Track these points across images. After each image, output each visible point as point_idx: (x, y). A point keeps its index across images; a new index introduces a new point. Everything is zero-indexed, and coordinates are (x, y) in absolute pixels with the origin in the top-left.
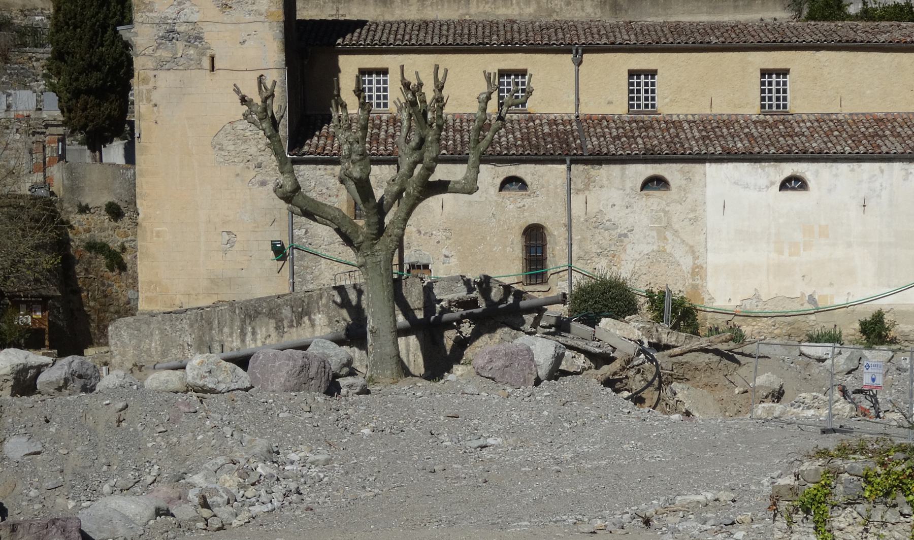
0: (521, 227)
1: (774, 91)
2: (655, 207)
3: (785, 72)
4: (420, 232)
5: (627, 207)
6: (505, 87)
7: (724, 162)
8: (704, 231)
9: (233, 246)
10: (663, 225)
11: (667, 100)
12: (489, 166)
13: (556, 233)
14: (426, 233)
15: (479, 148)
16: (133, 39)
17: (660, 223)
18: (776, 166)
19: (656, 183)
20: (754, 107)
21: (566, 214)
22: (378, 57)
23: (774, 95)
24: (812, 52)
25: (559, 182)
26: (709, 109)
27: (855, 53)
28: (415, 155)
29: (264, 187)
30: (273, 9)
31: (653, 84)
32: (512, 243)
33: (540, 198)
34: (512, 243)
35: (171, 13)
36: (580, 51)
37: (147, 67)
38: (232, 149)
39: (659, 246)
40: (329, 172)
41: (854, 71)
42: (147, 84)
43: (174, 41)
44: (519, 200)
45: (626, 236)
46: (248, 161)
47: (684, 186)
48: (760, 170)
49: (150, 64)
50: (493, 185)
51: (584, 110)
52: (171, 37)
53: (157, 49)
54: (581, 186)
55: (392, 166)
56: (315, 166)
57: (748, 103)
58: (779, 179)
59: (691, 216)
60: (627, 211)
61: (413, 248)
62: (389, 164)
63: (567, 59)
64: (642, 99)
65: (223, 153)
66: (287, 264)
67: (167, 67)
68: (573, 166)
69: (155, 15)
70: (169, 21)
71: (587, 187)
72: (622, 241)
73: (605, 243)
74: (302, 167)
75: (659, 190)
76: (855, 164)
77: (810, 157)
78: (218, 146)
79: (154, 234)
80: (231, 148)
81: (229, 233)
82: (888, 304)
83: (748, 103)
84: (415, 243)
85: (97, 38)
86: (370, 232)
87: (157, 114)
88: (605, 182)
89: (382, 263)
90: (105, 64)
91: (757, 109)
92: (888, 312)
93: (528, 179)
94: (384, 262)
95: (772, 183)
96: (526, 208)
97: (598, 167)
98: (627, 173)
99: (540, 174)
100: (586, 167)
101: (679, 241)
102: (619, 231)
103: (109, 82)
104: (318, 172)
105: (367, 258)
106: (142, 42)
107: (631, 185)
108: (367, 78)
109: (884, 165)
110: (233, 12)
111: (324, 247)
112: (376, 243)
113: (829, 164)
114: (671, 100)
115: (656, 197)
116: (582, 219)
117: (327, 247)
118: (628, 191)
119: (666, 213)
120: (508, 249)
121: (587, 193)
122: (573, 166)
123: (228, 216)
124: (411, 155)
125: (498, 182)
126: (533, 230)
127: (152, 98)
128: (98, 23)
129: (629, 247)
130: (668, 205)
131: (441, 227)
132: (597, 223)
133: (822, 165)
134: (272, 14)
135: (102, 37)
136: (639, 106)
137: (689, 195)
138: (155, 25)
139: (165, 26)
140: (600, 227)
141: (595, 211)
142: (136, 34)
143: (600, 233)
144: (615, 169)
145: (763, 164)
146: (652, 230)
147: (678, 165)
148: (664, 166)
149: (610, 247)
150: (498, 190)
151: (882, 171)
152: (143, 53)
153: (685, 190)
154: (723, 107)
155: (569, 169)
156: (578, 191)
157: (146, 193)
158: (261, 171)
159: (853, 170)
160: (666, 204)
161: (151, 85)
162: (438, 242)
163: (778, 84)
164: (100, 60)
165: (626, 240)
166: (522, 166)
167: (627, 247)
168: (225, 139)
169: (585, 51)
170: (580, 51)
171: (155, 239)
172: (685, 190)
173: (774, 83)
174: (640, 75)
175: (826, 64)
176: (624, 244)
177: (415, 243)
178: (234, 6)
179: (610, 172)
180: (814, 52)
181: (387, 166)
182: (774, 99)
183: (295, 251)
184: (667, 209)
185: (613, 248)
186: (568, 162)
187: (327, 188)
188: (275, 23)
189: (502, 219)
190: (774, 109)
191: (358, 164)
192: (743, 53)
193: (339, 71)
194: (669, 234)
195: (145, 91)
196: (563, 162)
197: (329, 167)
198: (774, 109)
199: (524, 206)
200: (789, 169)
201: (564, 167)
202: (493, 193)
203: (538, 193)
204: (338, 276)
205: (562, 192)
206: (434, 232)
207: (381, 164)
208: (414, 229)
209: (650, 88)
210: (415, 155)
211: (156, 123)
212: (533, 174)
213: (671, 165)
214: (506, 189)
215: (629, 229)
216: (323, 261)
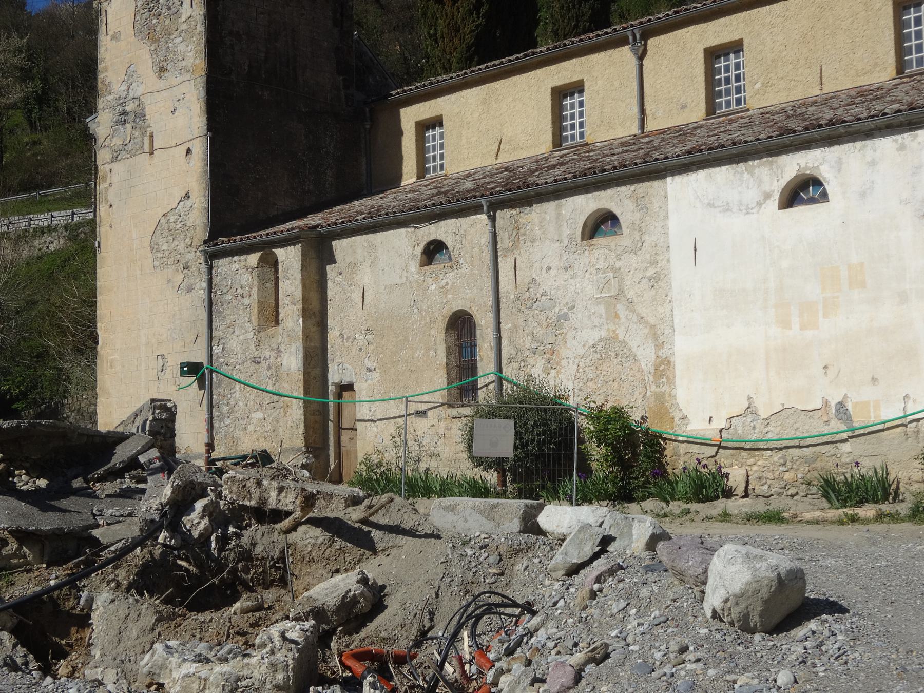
2: (601, 265)
5: (566, 269)
7: (692, 171)
10: (613, 294)
11: (758, 86)
12: (409, 229)
14: (349, 338)
20: (886, 69)
30: (198, 61)
33: (463, 270)
34: (435, 344)
40: (243, 264)
47: (638, 222)
48: (746, 175)
59: (650, 273)
71: (515, 246)
83: (876, 64)
95: (767, 196)
96: (448, 287)
97: (528, 209)
100: (514, 212)
101: (635, 319)
114: (763, 84)
116: (512, 297)
119: (616, 270)
137: (646, 237)
141: (527, 281)
145: (751, 163)
147: (628, 187)
150: (418, 265)
155: (493, 219)
159: (902, 148)
172: (640, 229)
174: (729, 54)
176: (565, 331)
181: (292, 247)
183: (214, 375)
199: (447, 284)
201: (483, 217)
205: (487, 256)
208: (338, 334)
216: (238, 385)
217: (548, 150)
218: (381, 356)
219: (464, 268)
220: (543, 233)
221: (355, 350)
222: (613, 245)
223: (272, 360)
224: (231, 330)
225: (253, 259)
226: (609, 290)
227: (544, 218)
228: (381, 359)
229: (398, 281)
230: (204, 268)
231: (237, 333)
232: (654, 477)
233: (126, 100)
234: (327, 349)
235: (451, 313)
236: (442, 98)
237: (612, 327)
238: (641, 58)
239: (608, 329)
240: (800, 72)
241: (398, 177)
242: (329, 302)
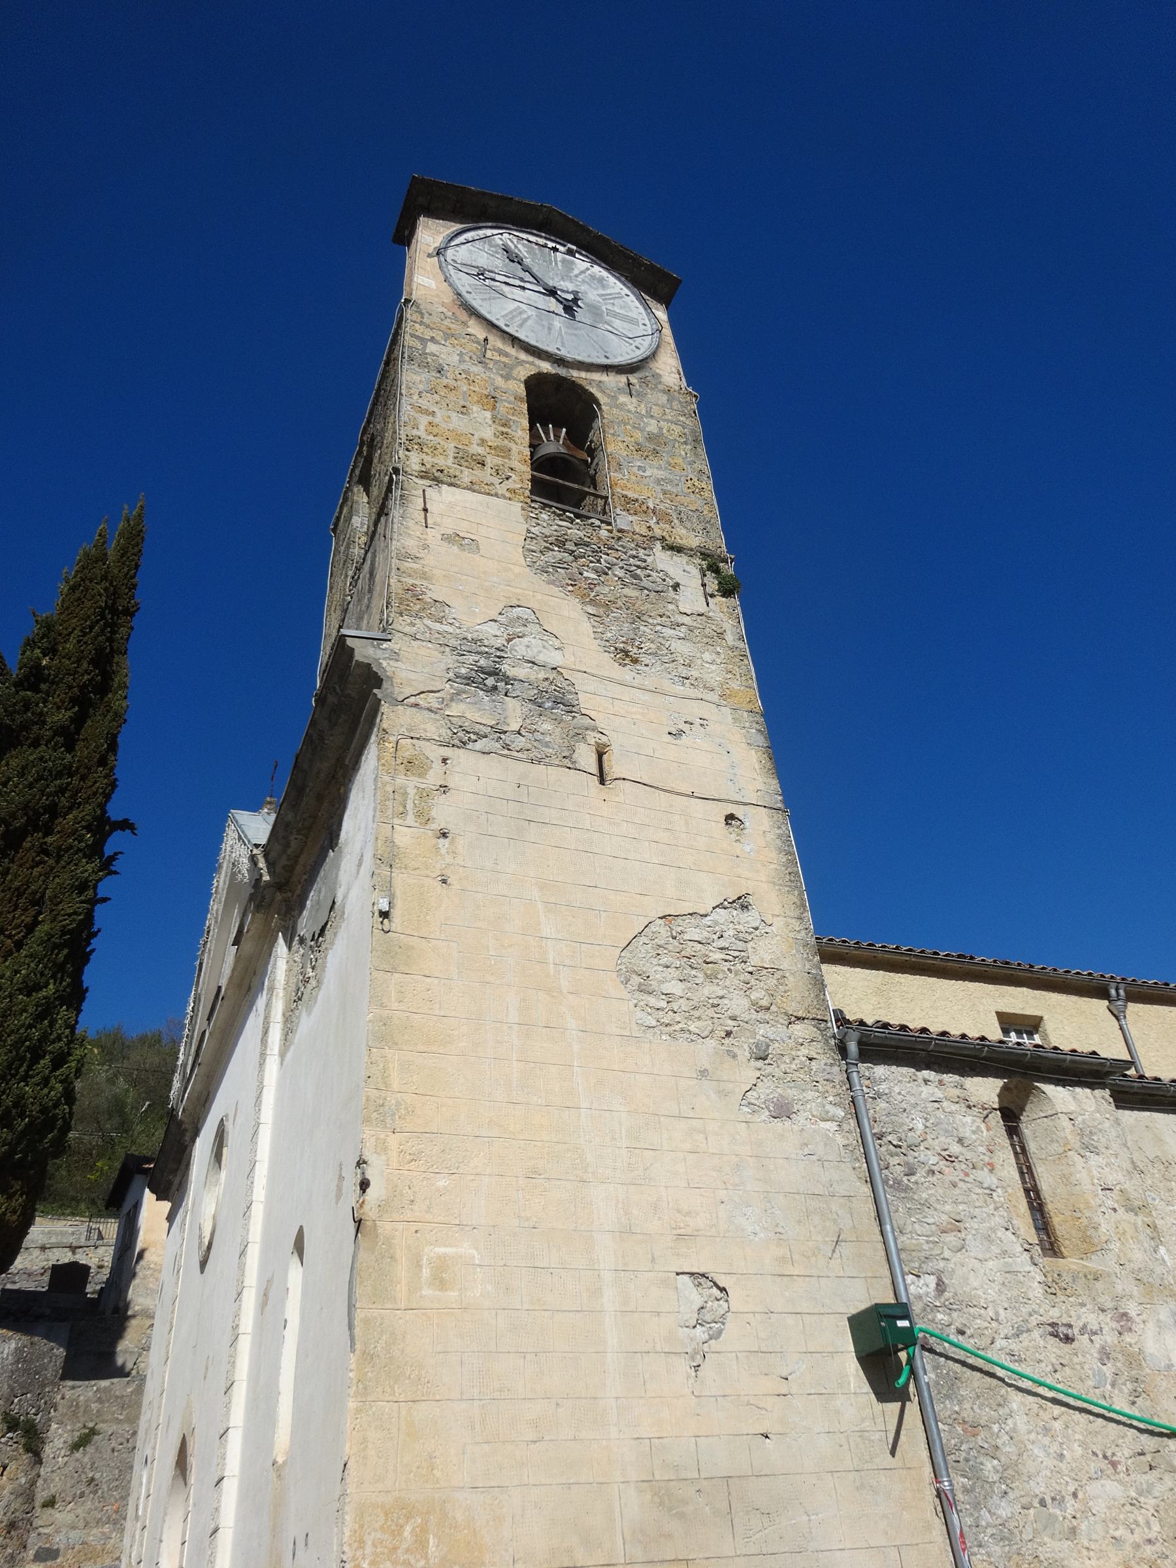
9: (720, 1332)
16: (384, 664)
35: (493, 634)
38: (679, 992)
46: (728, 1034)
49: (433, 728)
53: (452, 700)
55: (1098, 1092)
56: (913, 1070)
58: (1105, 1367)
65: (652, 1001)
66: (912, 1408)
67: (479, 745)
74: (880, 1070)
78: (636, 980)
79: (426, 1272)
80: (676, 988)
85: (21, 1066)
87: (449, 859)
90: (22, 1115)
103: (21, 1152)
106: (412, 676)
111: (1004, 1343)
123: (688, 1214)
127: (433, 813)
128: (27, 1043)
135: (30, 1068)
138: (447, 649)
142: (395, 656)
152: (412, 700)
157: (398, 1104)
158: (769, 1069)
161: (434, 777)
164: (16, 1105)
168: (655, 961)
171: (426, 1292)
181: (1088, 1091)
188: (745, 714)
195: (412, 792)
211: (444, 882)
216: (1016, 1399)
225: (987, 1089)
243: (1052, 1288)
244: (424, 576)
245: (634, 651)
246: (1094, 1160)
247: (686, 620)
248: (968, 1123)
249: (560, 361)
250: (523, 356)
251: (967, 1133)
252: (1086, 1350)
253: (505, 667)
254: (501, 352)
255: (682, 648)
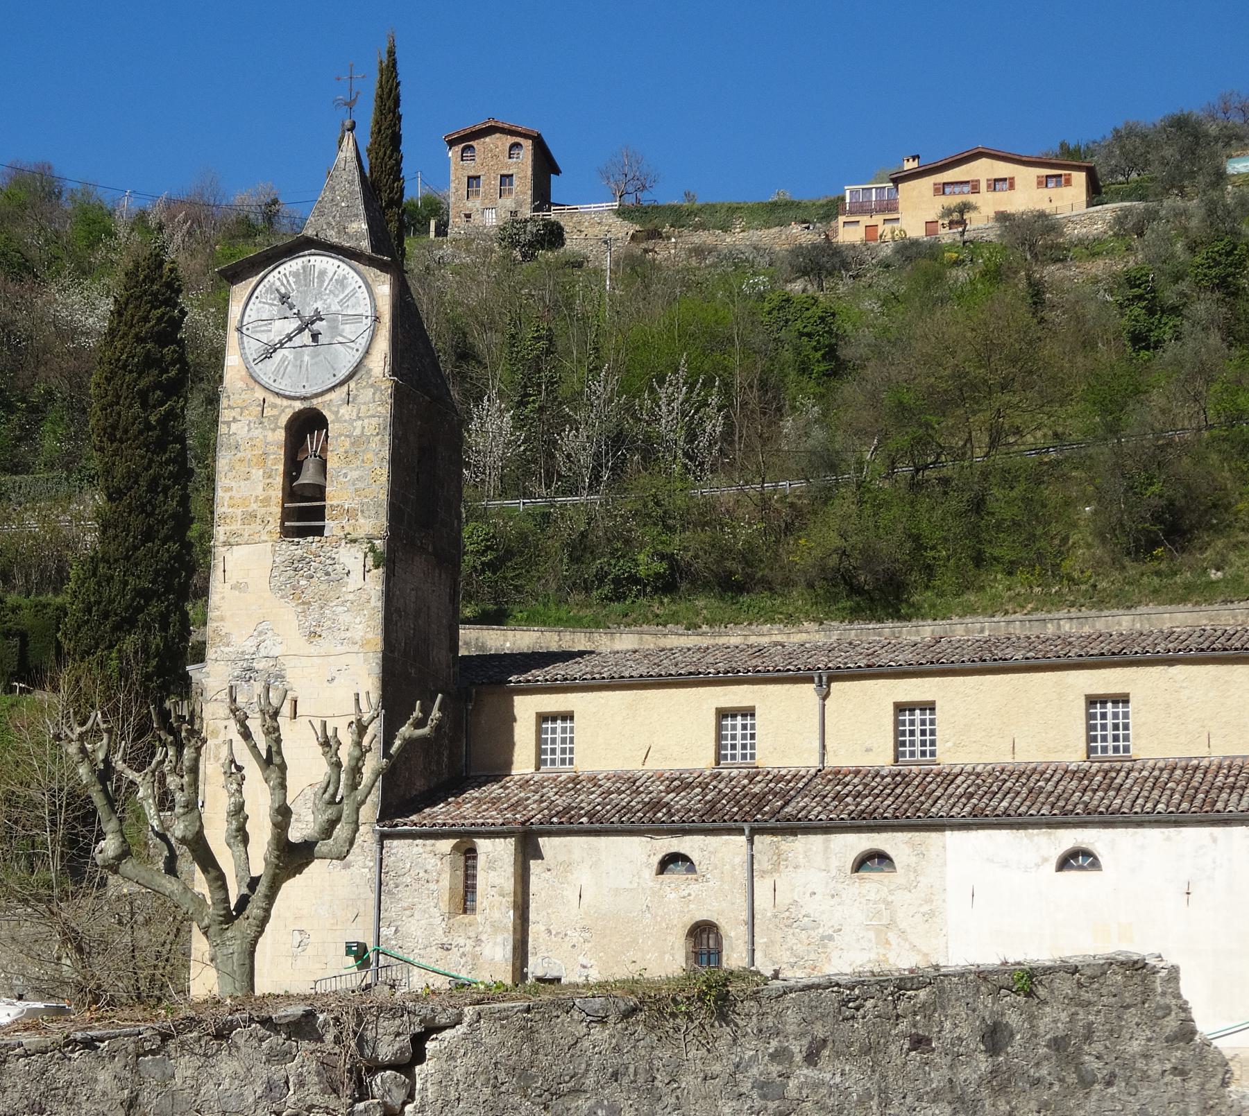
0: (684, 926)
1: (1110, 727)
2: (872, 896)
3: (1123, 699)
4: (550, 932)
5: (833, 896)
6: (729, 733)
7: (972, 829)
8: (944, 932)
10: (884, 922)
11: (949, 744)
12: (644, 839)
13: (732, 934)
14: (558, 933)
15: (356, 797)
17: (880, 919)
18: (1050, 833)
19: (873, 860)
20: (1076, 751)
21: (745, 905)
22: (554, 697)
23: (1110, 733)
24: (1162, 667)
25: (737, 860)
26: (1011, 756)
27: (1230, 666)
28: (330, 811)
29: (348, 870)
30: (370, 636)
31: (932, 722)
32: (673, 948)
33: (711, 884)
34: (673, 948)
35: (249, 646)
36: (824, 679)
37: (217, 716)
39: (878, 953)
40: (429, 848)
41: (1229, 693)
42: (217, 738)
43: (252, 681)
44: (683, 887)
45: (830, 938)
47: (913, 865)
48: (1025, 839)
50: (648, 865)
51: (832, 762)
52: (247, 676)
54: (767, 866)
57: (1067, 746)
59: (925, 908)
60: (833, 902)
61: (540, 955)
62: (505, 838)
63: (808, 691)
64: (918, 743)
68: (756, 838)
69: (231, 649)
70: (246, 657)
71: (776, 867)
72: (825, 946)
73: (800, 949)
74: (396, 843)
75: (882, 871)
76: (1172, 830)
77: (1097, 819)
81: (301, 931)
82: (1231, 1048)
83: (1067, 746)
84: (543, 948)
86: (216, 912)
88: (801, 860)
89: (236, 954)
91: (1081, 754)
92: (1231, 1060)
93: (694, 857)
94: (239, 954)
95: (1045, 860)
96: (691, 898)
97: (792, 838)
98: (832, 846)
99: (711, 849)
100: (775, 839)
101: (907, 946)
102: (821, 930)
104: (415, 850)
105: (217, 948)
107: (837, 864)
108: (549, 725)
109: (1218, 831)
110: (321, 641)
112: (227, 929)
113: (1131, 831)
114: (955, 744)
115: (874, 880)
116: (769, 914)
117: (422, 952)
118: (834, 872)
119: (888, 904)
120: (667, 956)
121: (776, 875)
122: (756, 838)
124: (325, 811)
125: (656, 860)
126: (705, 930)
129: (835, 955)
130: (891, 892)
131: (578, 925)
132: (789, 920)
133: (1120, 832)
134: (368, 642)
136: (912, 754)
137: (920, 878)
139: (242, 663)
140: (795, 925)
141: (787, 902)
143: (793, 934)
144: (816, 840)
145: (1030, 831)
146: (868, 930)
147: (905, 834)
148: (884, 835)
149: (808, 955)
150: (654, 872)
151: (1215, 840)
153: (915, 871)
154: (1030, 754)
155: (751, 841)
156: (764, 873)
159: (1168, 839)
160: (889, 891)
162: (574, 946)
163: (1115, 716)
165: (831, 944)
166: (687, 838)
167: (832, 955)
169: (832, 679)
170: (824, 679)
172: (915, 871)
173: (1109, 716)
174: (914, 710)
175: (1185, 685)
176: (829, 950)
177: (543, 948)
178: (324, 635)
179: (808, 846)
180: (1166, 667)
181: (502, 840)
182: (1110, 739)
183: (381, 957)
184: (890, 899)
185: (813, 956)
186: (747, 832)
187: (426, 871)
189: (660, 913)
190: (1110, 753)
191: (182, 818)
192: (1059, 673)
193: (514, 720)
194: (892, 936)
196: (740, 831)
197: (429, 842)
198: (1110, 753)
199: (689, 895)
200: (1069, 838)
201: (742, 839)
202: (647, 876)
203: (708, 876)
204: (318, 983)
205: (742, 875)
206: (569, 932)
207: (494, 838)
208: (543, 928)
209: (928, 727)
210: (330, 811)
212: (702, 850)
213: (895, 834)
214: (670, 870)
215: (837, 927)
216: (416, 970)
217: (709, 766)
218: (601, 954)
219: (712, 882)
220: (809, 862)
221: (567, 946)
222: (886, 881)
223: (467, 949)
224: (408, 913)
225: (446, 845)
226: (880, 919)
227: (810, 849)
228: (600, 957)
229: (628, 886)
230: (376, 847)
231: (416, 917)
232: (660, 1099)
233: (254, 656)
234: (527, 942)
235: (693, 922)
236: (574, 695)
237: (882, 951)
238: (824, 699)
239: (878, 953)
240: (992, 740)
241: (508, 764)
242: (531, 896)
243: (448, 931)
244: (222, 619)
245: (318, 630)
246: (492, 874)
247: (351, 597)
248: (431, 863)
249: (305, 399)
250: (286, 402)
251: (429, 867)
252: (455, 954)
253: (256, 665)
254: (274, 406)
255: (345, 618)
